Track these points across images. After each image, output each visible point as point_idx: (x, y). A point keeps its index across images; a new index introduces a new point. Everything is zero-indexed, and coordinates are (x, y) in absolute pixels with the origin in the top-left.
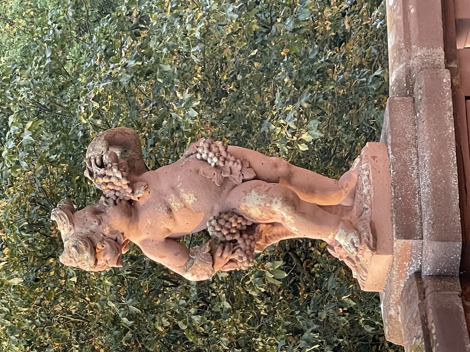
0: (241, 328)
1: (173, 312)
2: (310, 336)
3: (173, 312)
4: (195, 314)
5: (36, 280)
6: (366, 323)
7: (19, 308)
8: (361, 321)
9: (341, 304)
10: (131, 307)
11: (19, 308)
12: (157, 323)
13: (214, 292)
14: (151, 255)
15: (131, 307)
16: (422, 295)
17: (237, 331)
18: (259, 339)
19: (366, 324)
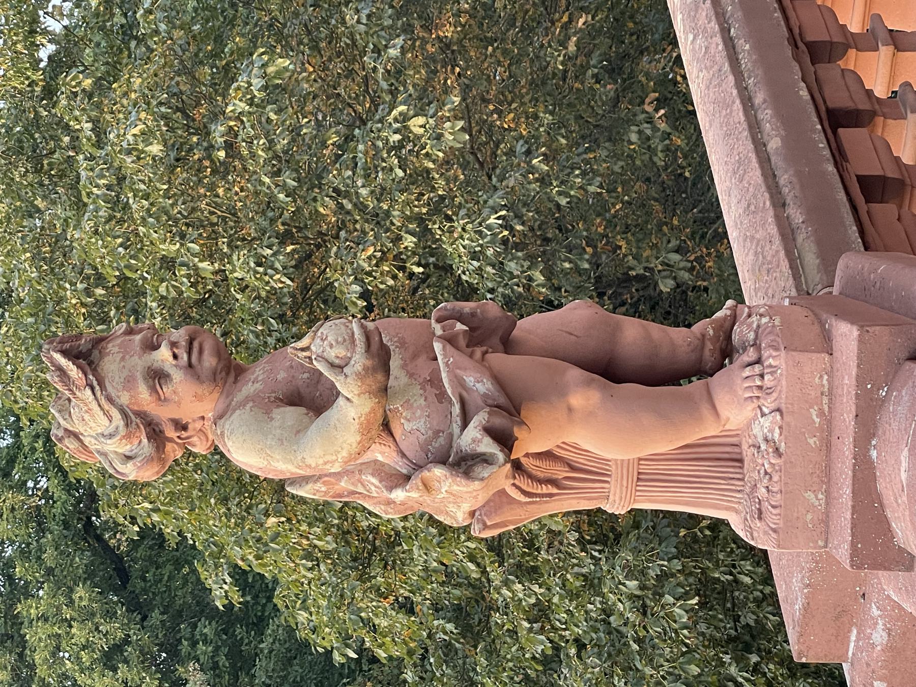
0: (415, 206)
1: (335, 190)
2: (495, 202)
3: (335, 190)
4: (363, 186)
5: (177, 160)
6: (560, 193)
7: (158, 185)
8: (554, 192)
9: (532, 169)
10: (288, 181)
11: (158, 185)
12: (319, 203)
13: (384, 160)
14: (389, 504)
15: (288, 181)
16: (692, 14)
17: (412, 211)
18: (436, 226)
19: (560, 195)
